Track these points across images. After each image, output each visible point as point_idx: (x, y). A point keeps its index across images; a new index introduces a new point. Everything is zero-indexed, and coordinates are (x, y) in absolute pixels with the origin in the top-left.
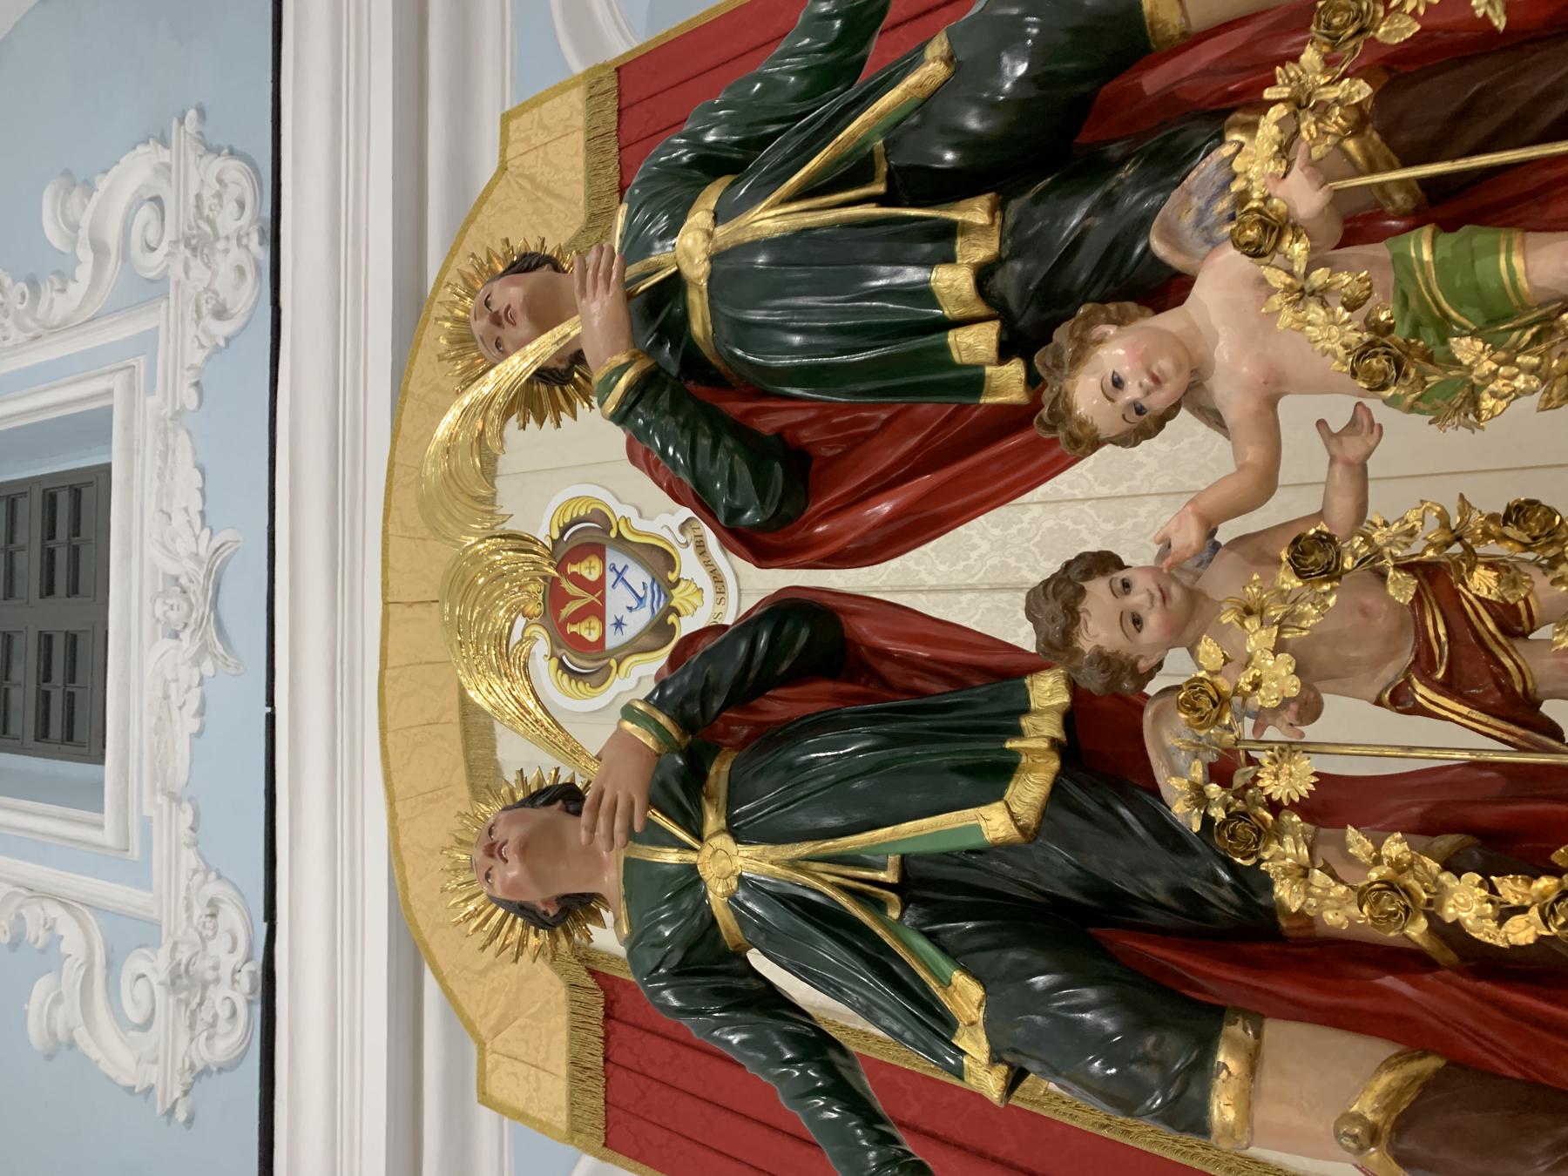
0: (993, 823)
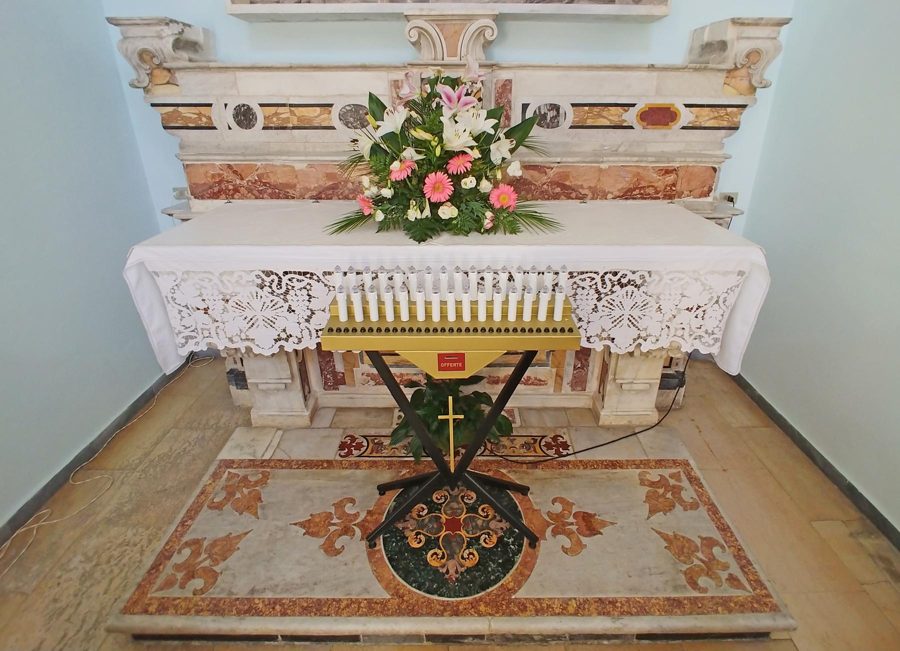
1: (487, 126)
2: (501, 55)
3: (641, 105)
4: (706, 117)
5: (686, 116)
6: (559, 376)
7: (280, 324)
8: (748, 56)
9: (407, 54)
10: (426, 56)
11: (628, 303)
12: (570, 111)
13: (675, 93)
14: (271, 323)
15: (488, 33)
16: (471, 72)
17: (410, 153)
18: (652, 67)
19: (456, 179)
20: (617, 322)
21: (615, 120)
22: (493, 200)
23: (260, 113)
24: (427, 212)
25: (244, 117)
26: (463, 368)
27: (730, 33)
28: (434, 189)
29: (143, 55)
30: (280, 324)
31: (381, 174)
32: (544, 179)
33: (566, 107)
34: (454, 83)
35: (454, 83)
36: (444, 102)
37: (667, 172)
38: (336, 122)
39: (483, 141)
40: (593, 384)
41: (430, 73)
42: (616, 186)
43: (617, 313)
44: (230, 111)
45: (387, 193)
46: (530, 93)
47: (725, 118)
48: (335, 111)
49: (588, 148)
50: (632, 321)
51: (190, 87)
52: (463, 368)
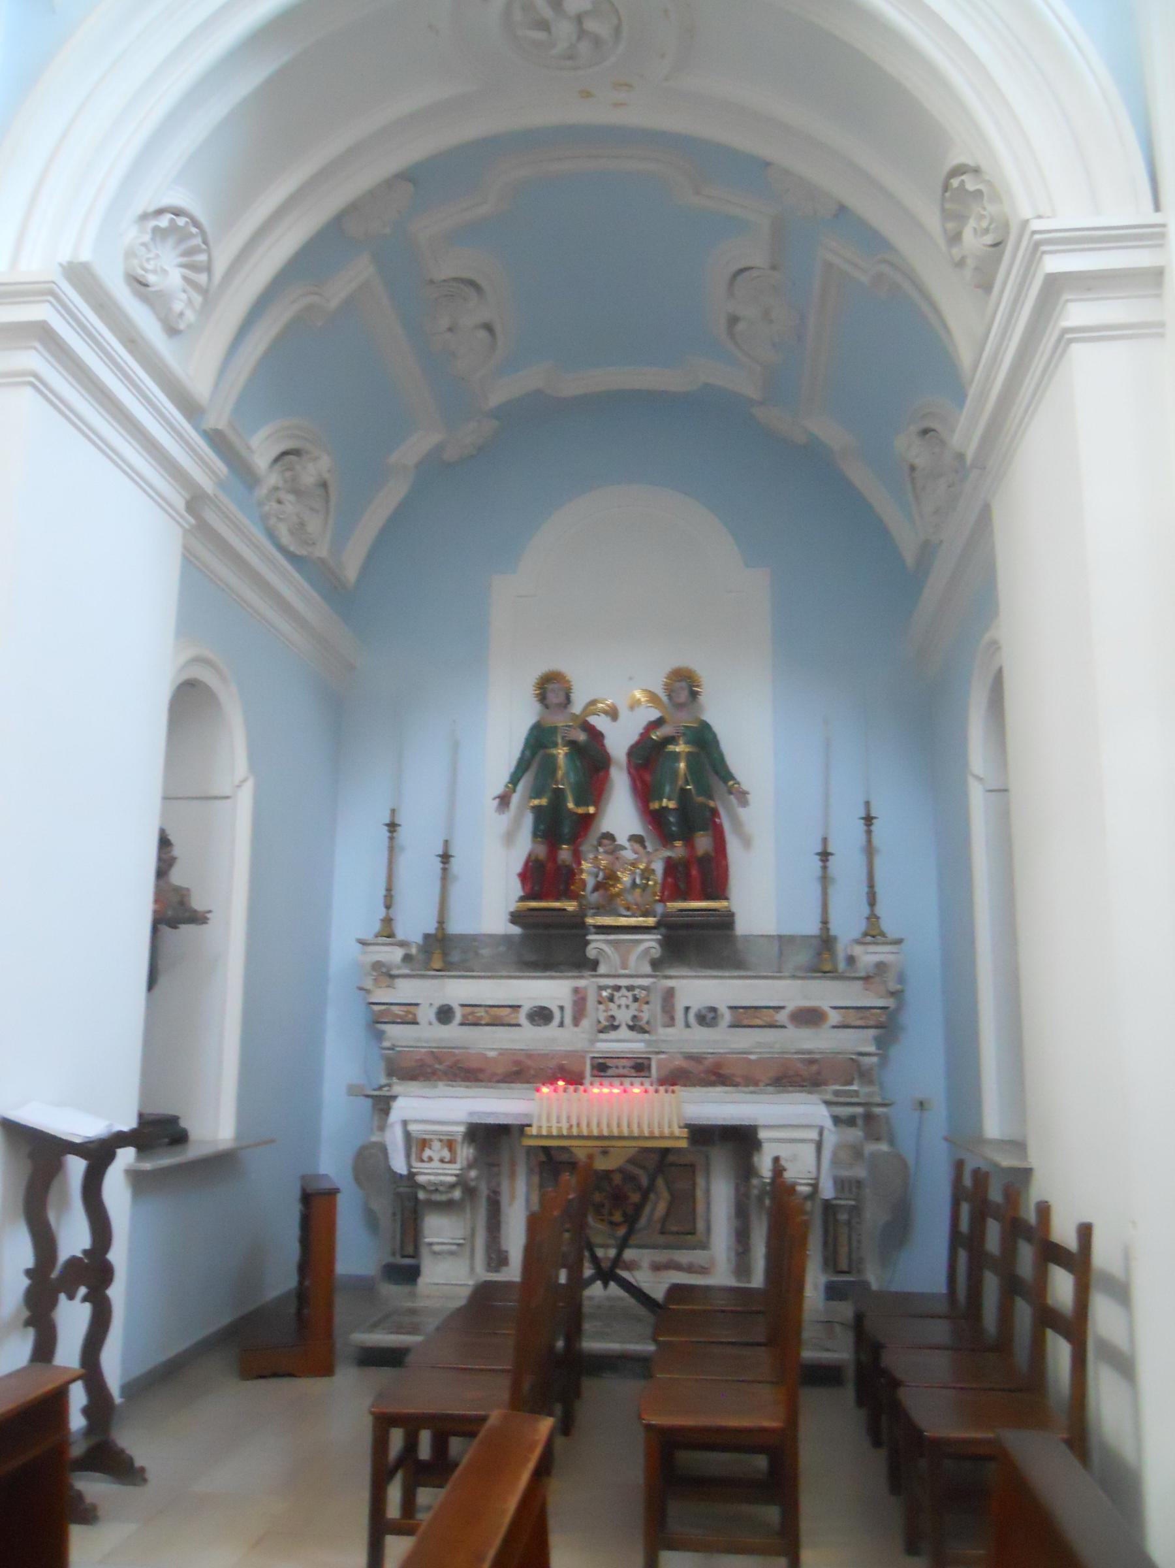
0: (571, 805)
3: (791, 1006)
5: (834, 1017)
25: (445, 1014)
29: (377, 966)
44: (434, 1010)
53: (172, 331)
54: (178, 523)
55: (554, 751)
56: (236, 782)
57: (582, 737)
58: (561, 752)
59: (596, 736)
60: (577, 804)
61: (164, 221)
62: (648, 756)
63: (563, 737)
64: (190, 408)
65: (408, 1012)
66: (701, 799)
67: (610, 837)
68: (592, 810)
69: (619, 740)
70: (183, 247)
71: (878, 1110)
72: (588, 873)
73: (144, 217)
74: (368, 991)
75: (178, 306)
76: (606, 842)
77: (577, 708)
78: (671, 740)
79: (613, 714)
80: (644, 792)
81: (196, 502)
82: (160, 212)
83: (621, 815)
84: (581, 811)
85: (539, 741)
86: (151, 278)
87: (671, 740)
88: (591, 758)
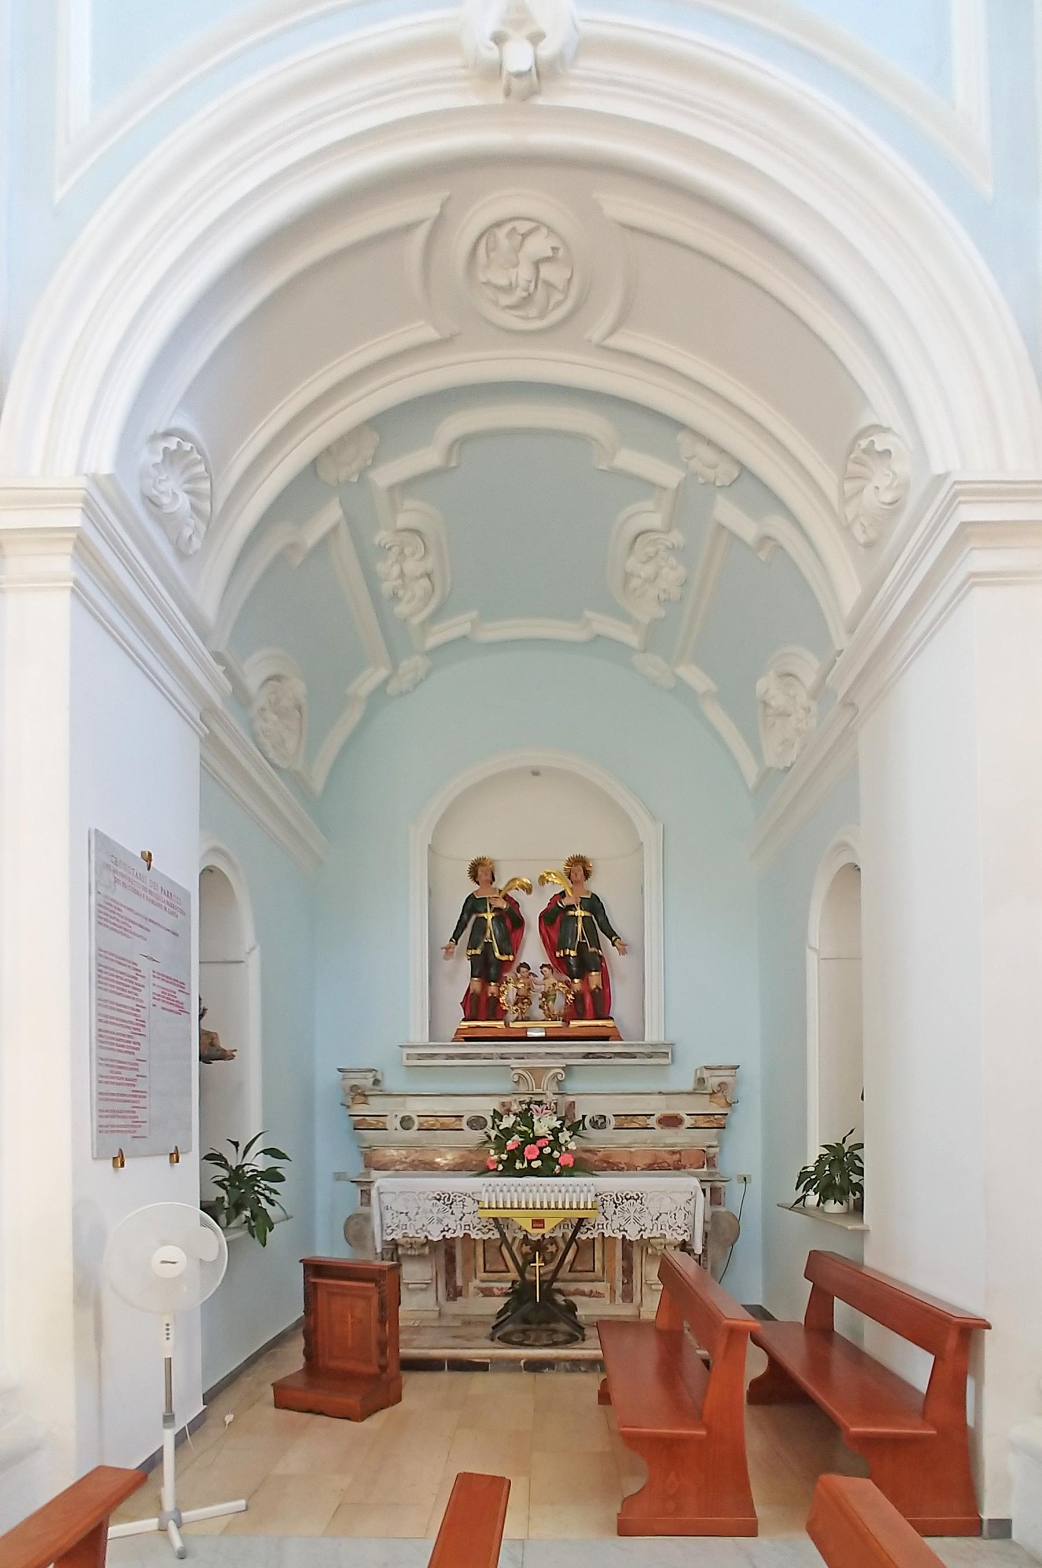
0: (497, 954)
1: (558, 1124)
2: (573, 1086)
3: (658, 1115)
4: (702, 1122)
5: (688, 1121)
6: (613, 1290)
7: (445, 1222)
8: (719, 1085)
9: (507, 1086)
10: (523, 1088)
11: (632, 1210)
12: (613, 1119)
13: (681, 1108)
14: (440, 1221)
15: (559, 1076)
16: (550, 1098)
17: (516, 1137)
18: (660, 1093)
19: (541, 1149)
20: (628, 1220)
21: (643, 1124)
22: (560, 1161)
23: (417, 1120)
24: (525, 1165)
25: (406, 1123)
26: (543, 1227)
27: (706, 1074)
28: (529, 1152)
29: (354, 1088)
30: (445, 1222)
31: (500, 1148)
32: (596, 1158)
33: (609, 1116)
34: (540, 1103)
35: (540, 1103)
36: (535, 1113)
37: (673, 1153)
38: (465, 1126)
39: (555, 1132)
40: (637, 1298)
41: (527, 1098)
42: (640, 1162)
43: (627, 1215)
44: (398, 1120)
45: (504, 1157)
46: (586, 1109)
47: (718, 1123)
48: (465, 1120)
49: (625, 1141)
50: (636, 1221)
51: (376, 1106)
52: (543, 1227)
53: (182, 555)
54: (197, 733)
55: (485, 915)
56: (247, 950)
57: (504, 905)
58: (489, 916)
59: (514, 904)
60: (501, 953)
61: (172, 443)
62: (554, 917)
63: (491, 906)
64: (204, 634)
65: (378, 1121)
66: (593, 949)
67: (525, 965)
68: (511, 958)
69: (532, 909)
70: (186, 475)
71: (718, 1184)
72: (509, 994)
73: (154, 438)
74: (348, 1107)
75: (187, 532)
76: (523, 969)
77: (501, 884)
78: (572, 907)
79: (528, 889)
80: (551, 945)
81: (208, 711)
82: (167, 434)
83: (533, 950)
84: (504, 958)
85: (473, 905)
86: (166, 500)
87: (572, 907)
88: (511, 920)
